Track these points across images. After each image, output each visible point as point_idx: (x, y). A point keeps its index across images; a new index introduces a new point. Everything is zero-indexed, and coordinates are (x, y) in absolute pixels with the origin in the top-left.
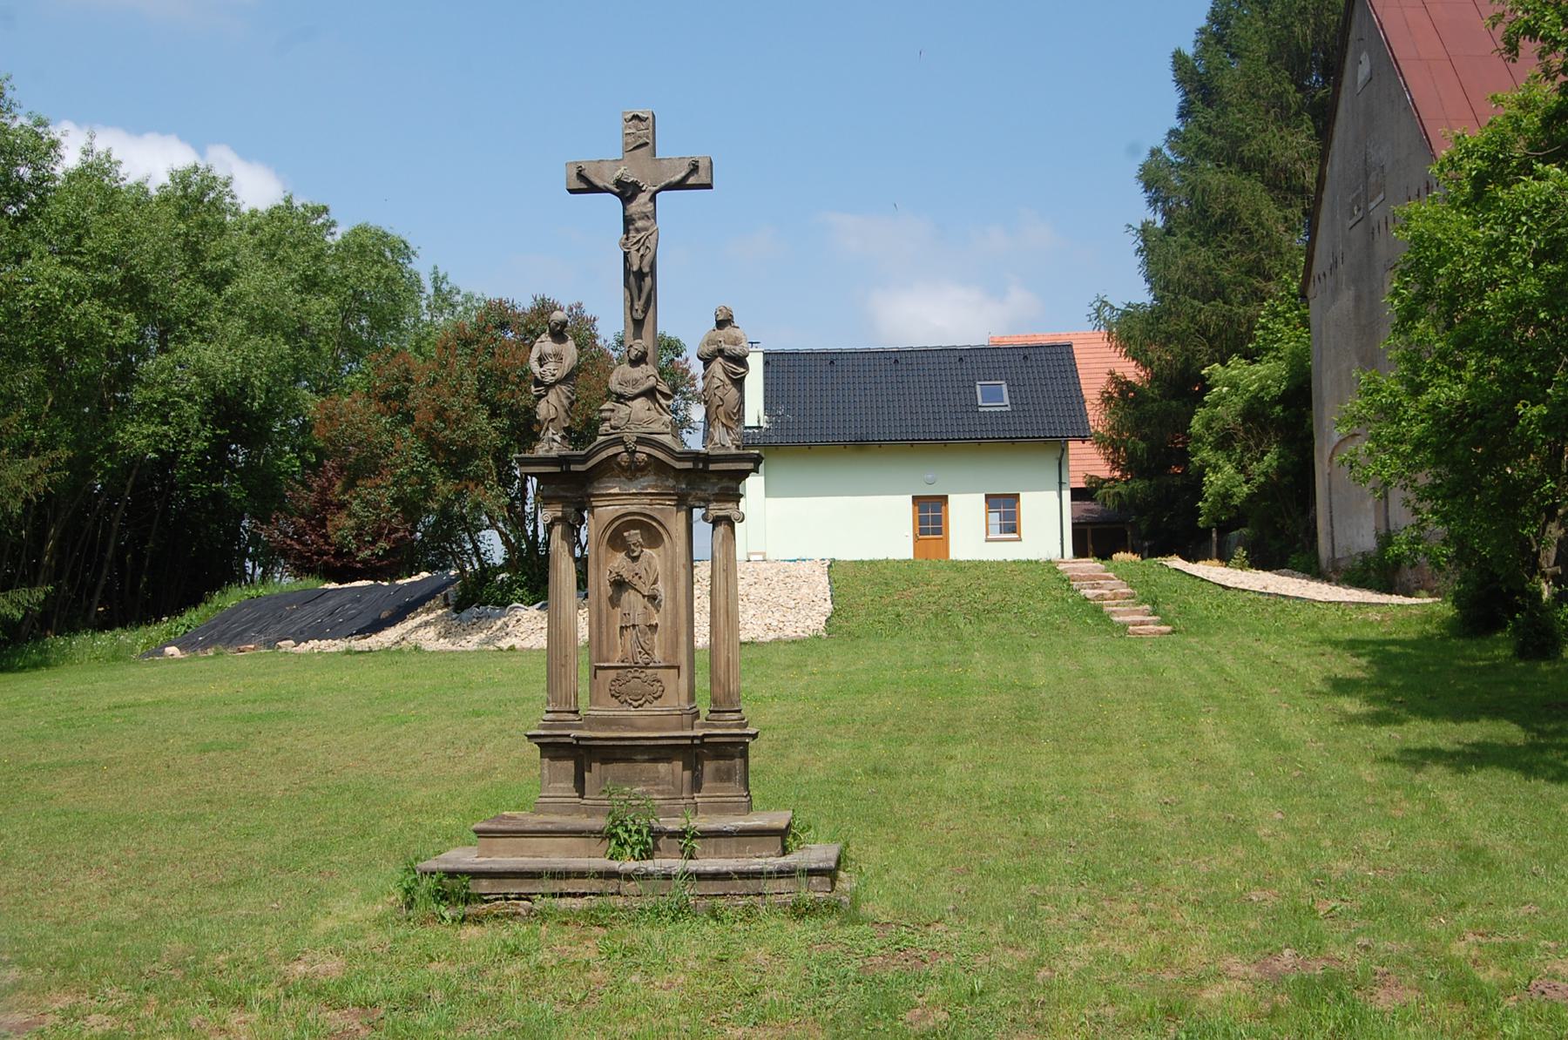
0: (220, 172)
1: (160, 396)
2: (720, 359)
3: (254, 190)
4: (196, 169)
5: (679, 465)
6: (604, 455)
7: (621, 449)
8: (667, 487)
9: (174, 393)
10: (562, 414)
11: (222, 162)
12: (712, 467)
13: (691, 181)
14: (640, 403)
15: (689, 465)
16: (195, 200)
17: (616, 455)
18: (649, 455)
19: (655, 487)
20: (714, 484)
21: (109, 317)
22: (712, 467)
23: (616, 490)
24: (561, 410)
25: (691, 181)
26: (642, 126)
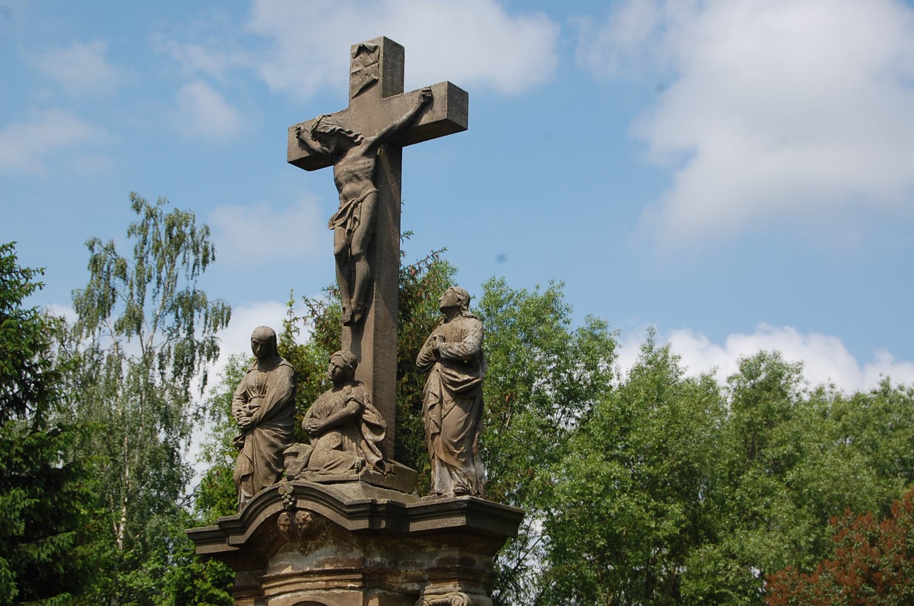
0: (789, 358)
1: (706, 589)
2: (438, 365)
3: (825, 371)
4: (761, 358)
5: (352, 525)
6: (261, 518)
7: (278, 507)
8: (351, 561)
9: (722, 585)
10: (262, 469)
11: (788, 349)
12: (414, 527)
13: (425, 119)
14: (330, 439)
15: (363, 524)
16: (765, 387)
17: (276, 516)
18: (314, 514)
19: (336, 561)
20: (432, 555)
21: (655, 509)
22: (414, 527)
23: (288, 570)
24: (260, 464)
25: (425, 119)
26: (370, 59)
